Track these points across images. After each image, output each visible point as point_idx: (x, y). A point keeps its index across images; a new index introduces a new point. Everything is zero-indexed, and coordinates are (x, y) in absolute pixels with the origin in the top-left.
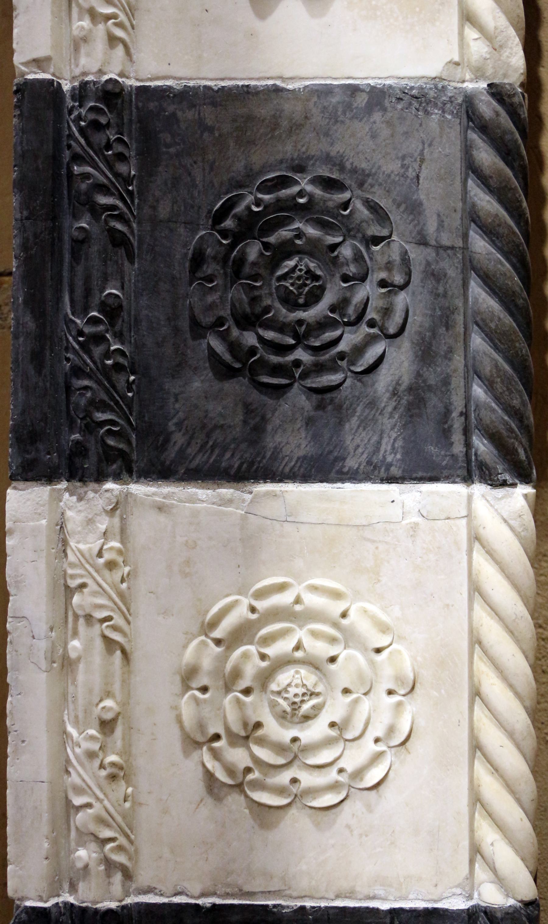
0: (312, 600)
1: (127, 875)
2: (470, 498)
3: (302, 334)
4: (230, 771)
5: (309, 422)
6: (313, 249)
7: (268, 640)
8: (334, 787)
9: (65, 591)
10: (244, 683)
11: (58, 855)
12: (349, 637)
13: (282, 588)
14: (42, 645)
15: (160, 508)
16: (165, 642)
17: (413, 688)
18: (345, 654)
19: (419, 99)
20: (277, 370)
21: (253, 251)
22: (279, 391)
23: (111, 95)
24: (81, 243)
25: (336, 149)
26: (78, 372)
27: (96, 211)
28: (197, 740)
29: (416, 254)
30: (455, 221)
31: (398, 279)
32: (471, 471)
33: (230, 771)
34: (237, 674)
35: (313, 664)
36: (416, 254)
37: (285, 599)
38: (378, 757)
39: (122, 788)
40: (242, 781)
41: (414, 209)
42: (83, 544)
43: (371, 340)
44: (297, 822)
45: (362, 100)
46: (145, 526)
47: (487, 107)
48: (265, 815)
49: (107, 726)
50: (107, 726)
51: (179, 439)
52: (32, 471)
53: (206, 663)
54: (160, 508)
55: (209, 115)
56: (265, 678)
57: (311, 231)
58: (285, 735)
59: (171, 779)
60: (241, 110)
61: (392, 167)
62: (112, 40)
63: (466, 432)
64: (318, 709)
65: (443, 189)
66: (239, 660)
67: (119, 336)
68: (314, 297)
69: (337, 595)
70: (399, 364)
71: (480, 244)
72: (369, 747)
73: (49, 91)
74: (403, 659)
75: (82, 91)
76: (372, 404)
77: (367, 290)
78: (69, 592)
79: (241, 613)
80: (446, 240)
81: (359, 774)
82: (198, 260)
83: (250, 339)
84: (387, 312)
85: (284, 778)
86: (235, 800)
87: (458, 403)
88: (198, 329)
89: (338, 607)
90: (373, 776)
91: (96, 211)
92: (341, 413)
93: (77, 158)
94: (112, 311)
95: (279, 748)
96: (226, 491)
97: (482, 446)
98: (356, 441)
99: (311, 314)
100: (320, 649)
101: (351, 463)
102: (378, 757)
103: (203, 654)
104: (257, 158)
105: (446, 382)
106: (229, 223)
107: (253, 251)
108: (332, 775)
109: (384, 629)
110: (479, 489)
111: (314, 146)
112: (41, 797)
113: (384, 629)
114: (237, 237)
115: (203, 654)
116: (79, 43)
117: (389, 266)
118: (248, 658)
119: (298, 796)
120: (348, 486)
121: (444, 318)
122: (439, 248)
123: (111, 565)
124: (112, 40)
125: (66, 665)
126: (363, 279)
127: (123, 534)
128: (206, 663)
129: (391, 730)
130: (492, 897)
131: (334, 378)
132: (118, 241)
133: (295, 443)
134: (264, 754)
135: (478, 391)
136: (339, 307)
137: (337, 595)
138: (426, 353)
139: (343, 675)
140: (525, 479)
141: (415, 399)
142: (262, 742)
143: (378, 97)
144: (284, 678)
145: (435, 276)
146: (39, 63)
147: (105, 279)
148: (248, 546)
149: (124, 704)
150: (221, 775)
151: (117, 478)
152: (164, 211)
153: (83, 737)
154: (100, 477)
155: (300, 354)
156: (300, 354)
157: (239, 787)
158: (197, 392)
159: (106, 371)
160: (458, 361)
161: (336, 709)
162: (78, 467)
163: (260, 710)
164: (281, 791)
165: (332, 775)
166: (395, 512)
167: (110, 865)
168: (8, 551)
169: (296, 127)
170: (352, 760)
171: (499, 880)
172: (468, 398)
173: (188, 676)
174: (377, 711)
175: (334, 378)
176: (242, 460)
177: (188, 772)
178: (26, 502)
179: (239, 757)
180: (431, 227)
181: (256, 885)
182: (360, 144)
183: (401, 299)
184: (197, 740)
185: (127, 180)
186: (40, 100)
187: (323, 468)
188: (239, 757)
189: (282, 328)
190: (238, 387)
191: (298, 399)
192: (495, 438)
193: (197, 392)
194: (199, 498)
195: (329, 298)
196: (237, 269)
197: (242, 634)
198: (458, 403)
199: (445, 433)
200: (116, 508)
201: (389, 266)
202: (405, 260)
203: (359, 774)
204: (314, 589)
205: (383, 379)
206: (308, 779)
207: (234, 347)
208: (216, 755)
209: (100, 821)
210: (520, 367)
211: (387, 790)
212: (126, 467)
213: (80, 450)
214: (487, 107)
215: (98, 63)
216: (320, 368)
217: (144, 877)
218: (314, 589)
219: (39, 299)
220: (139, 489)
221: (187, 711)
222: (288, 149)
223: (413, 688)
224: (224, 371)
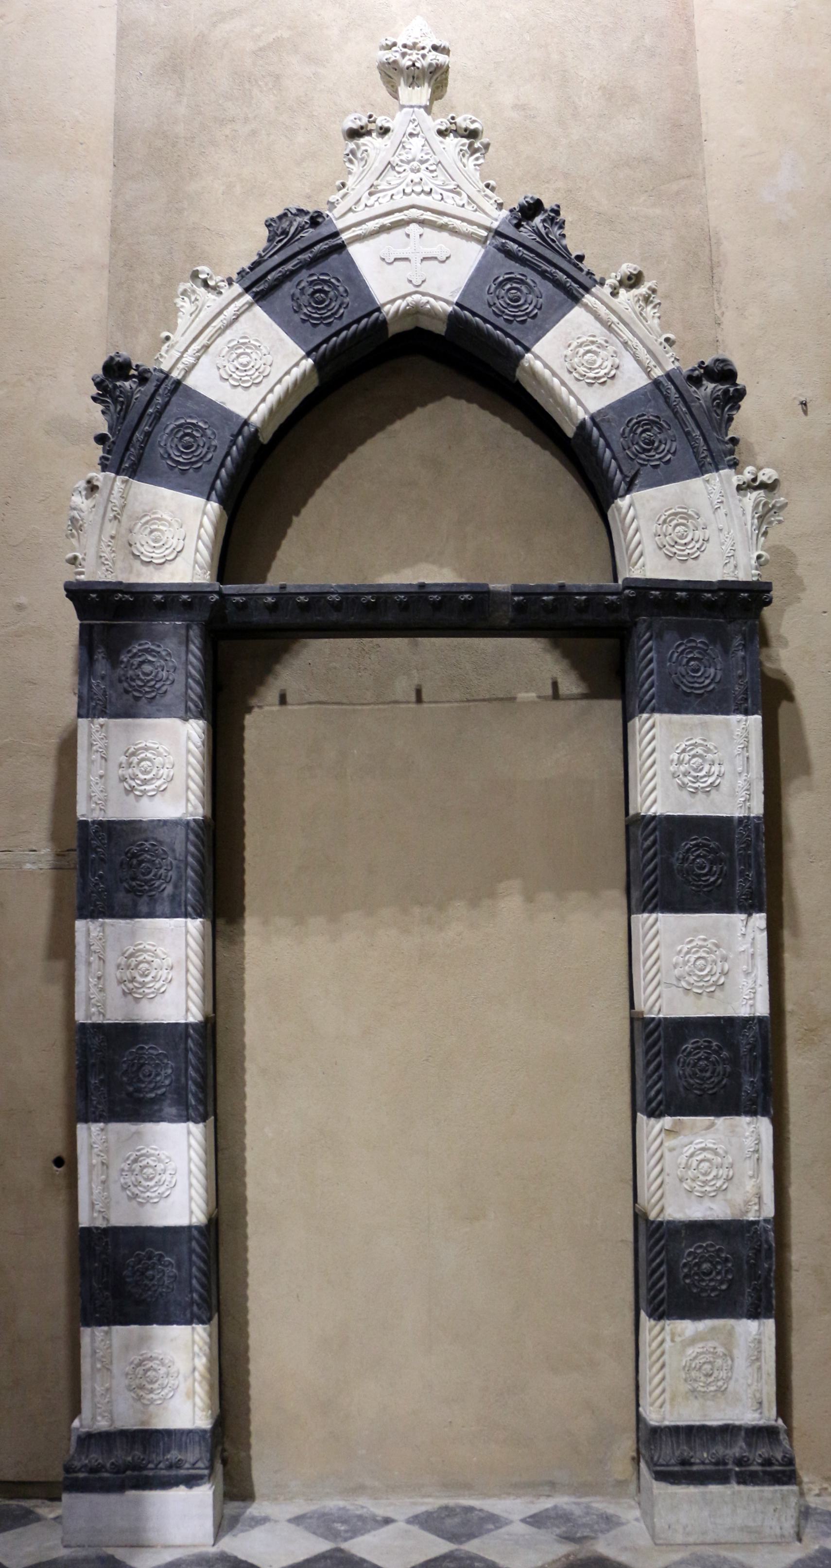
0: (148, 947)
1: (104, 1015)
2: (186, 922)
3: (146, 882)
4: (128, 989)
5: (148, 904)
6: (149, 861)
7: (137, 957)
8: (153, 993)
9: (89, 945)
10: (132, 967)
11: (87, 1010)
12: (157, 956)
13: (141, 944)
14: (84, 959)
15: (112, 925)
16: (113, 957)
17: (172, 780)
18: (158, 1165)
19: (176, 823)
20: (140, 891)
21: (135, 862)
22: (140, 896)
23: (101, 823)
24: (93, 860)
25: (155, 836)
26: (93, 892)
27: (97, 853)
28: (121, 982)
29: (174, 862)
30: (183, 854)
31: (169, 868)
32: (186, 915)
33: (128, 989)
34: (130, 965)
35: (148, 962)
36: (174, 862)
37: (141, 947)
38: (163, 985)
39: (102, 994)
40: (132, 991)
41: (173, 851)
42: (93, 934)
43: (162, 884)
44: (144, 1002)
45: (161, 823)
46: (108, 930)
47: (192, 824)
48: (137, 1000)
49: (99, 978)
50: (99, 978)
51: (117, 908)
52: (82, 916)
53: (123, 963)
54: (112, 925)
55: (124, 827)
56: (137, 966)
57: (149, 857)
58: (141, 980)
59: (114, 991)
60: (133, 827)
61: (168, 840)
62: (101, 809)
63: (186, 906)
64: (149, 974)
65: (182, 847)
66: (131, 961)
67: (103, 883)
68: (149, 873)
69: (154, 946)
70: (169, 889)
71: (190, 859)
72: (161, 982)
73: (85, 823)
74: (170, 961)
75: (94, 822)
76: (163, 899)
77: (162, 871)
78: (91, 946)
79: (131, 950)
80: (181, 858)
81: (159, 989)
82: (122, 864)
83: (134, 883)
84: (166, 876)
85: (141, 990)
86: (130, 997)
87: (183, 898)
88: (122, 881)
89: (154, 949)
90: (162, 990)
91: (97, 853)
92: (155, 901)
93: (92, 839)
94: (100, 876)
95: (140, 983)
96: (128, 921)
97: (190, 909)
98: (159, 909)
99: (148, 877)
100: (150, 959)
101: (158, 914)
102: (163, 985)
103: (122, 960)
104: (136, 838)
105: (180, 894)
106: (129, 855)
107: (135, 862)
108: (152, 990)
109: (165, 954)
110: (189, 920)
111: (150, 835)
112: (83, 995)
113: (165, 954)
114: (131, 858)
115: (122, 960)
116: (93, 810)
117: (167, 865)
118: (133, 961)
119: (145, 995)
120: (157, 920)
121: (180, 878)
122: (180, 860)
123: (100, 939)
124: (101, 809)
125: (89, 964)
126: (161, 868)
127: (103, 931)
128: (123, 963)
129: (167, 978)
130: (191, 1020)
131: (153, 893)
132: (102, 860)
133: (144, 909)
134: (136, 984)
135: (189, 896)
136: (155, 875)
137: (154, 946)
138: (176, 886)
139: (155, 965)
140: (201, 917)
141: (173, 898)
142: (137, 982)
143: (165, 823)
144: (141, 966)
145: (178, 867)
146: (83, 816)
147: (99, 870)
148: (133, 934)
149: (103, 972)
150: (127, 991)
151: (102, 918)
152: (114, 851)
153: (93, 981)
154: (98, 918)
155: (146, 887)
156: (146, 887)
157: (130, 993)
158: (121, 896)
159: (99, 892)
160: (184, 888)
161: (153, 974)
162: (93, 915)
163: (136, 974)
164: (140, 994)
165: (152, 990)
166: (168, 925)
167: (100, 1013)
168: (76, 929)
169: (145, 830)
170: (157, 986)
171: (194, 1016)
172: (186, 897)
173: (118, 966)
174: (163, 973)
175: (153, 893)
176: (132, 913)
177: (118, 990)
178: (80, 924)
179: (130, 986)
180: (178, 855)
181: (135, 1017)
182: (162, 834)
183: (170, 873)
184: (121, 982)
185: (104, 844)
186: (84, 825)
187: (151, 915)
188: (130, 986)
189: (141, 881)
190: (130, 895)
191: (145, 898)
192: (193, 907)
193: (121, 896)
194: (121, 923)
195: (152, 873)
196: (131, 866)
197: (132, 955)
198: (183, 898)
199: (180, 906)
200: (102, 925)
201: (167, 865)
202: (171, 863)
203: (159, 989)
204: (149, 944)
205: (166, 893)
206: (147, 991)
207: (130, 886)
208: (125, 985)
209: (98, 1001)
210: (199, 889)
211: (166, 994)
212: (103, 714)
213: (93, 911)
214: (192, 824)
215: (98, 816)
216: (150, 891)
217: (108, 1016)
218: (149, 944)
219: (83, 875)
220: (107, 921)
221: (118, 974)
222: (144, 836)
223: (172, 780)
224: (128, 891)
